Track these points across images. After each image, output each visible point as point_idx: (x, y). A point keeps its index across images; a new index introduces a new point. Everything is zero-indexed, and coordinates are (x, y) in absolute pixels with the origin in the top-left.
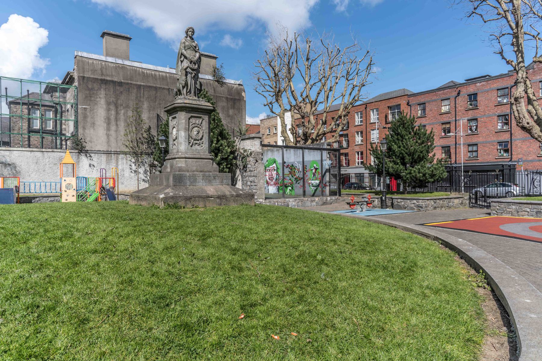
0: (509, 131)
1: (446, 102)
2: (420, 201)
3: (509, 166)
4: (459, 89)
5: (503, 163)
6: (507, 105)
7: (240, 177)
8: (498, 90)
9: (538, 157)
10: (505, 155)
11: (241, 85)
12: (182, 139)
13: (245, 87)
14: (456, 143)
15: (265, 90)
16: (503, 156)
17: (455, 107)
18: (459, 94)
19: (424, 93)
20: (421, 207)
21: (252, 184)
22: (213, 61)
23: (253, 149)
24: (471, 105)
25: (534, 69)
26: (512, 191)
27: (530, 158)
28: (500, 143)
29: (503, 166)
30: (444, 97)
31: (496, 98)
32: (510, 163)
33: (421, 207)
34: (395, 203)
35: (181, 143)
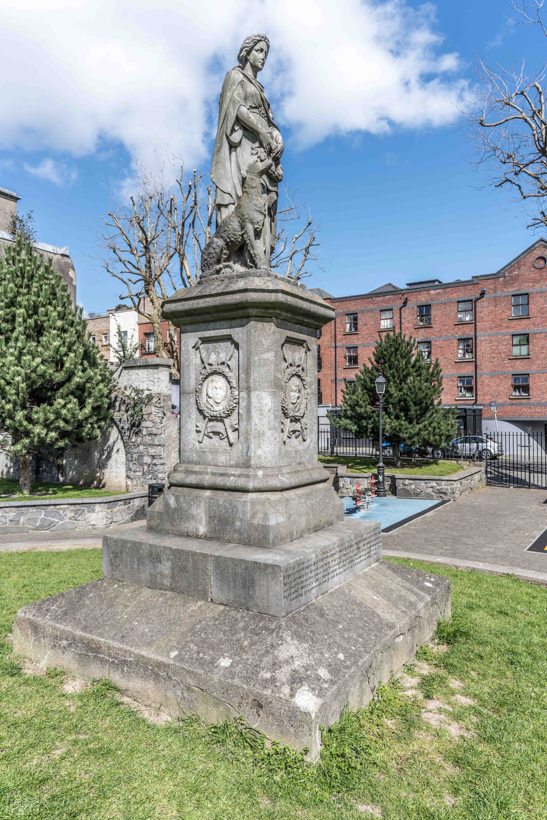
0: (473, 361)
1: (388, 315)
2: (443, 483)
3: (473, 411)
4: (405, 296)
5: (466, 407)
6: (470, 325)
7: (120, 445)
8: (458, 302)
9: (510, 399)
10: (467, 395)
11: (67, 256)
12: (265, 421)
13: (74, 260)
14: (336, 378)
15: (128, 271)
16: (465, 396)
17: (400, 322)
18: (405, 303)
19: (355, 298)
20: (445, 493)
21: (155, 461)
22: (10, 205)
23: (155, 390)
24: (421, 321)
25: (505, 277)
26: (489, 448)
27: (500, 401)
28: (461, 378)
29: (465, 410)
30: (385, 306)
31: (456, 314)
32: (475, 407)
33: (445, 493)
34: (400, 485)
35: (260, 435)
